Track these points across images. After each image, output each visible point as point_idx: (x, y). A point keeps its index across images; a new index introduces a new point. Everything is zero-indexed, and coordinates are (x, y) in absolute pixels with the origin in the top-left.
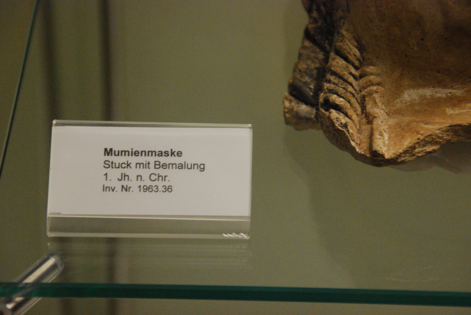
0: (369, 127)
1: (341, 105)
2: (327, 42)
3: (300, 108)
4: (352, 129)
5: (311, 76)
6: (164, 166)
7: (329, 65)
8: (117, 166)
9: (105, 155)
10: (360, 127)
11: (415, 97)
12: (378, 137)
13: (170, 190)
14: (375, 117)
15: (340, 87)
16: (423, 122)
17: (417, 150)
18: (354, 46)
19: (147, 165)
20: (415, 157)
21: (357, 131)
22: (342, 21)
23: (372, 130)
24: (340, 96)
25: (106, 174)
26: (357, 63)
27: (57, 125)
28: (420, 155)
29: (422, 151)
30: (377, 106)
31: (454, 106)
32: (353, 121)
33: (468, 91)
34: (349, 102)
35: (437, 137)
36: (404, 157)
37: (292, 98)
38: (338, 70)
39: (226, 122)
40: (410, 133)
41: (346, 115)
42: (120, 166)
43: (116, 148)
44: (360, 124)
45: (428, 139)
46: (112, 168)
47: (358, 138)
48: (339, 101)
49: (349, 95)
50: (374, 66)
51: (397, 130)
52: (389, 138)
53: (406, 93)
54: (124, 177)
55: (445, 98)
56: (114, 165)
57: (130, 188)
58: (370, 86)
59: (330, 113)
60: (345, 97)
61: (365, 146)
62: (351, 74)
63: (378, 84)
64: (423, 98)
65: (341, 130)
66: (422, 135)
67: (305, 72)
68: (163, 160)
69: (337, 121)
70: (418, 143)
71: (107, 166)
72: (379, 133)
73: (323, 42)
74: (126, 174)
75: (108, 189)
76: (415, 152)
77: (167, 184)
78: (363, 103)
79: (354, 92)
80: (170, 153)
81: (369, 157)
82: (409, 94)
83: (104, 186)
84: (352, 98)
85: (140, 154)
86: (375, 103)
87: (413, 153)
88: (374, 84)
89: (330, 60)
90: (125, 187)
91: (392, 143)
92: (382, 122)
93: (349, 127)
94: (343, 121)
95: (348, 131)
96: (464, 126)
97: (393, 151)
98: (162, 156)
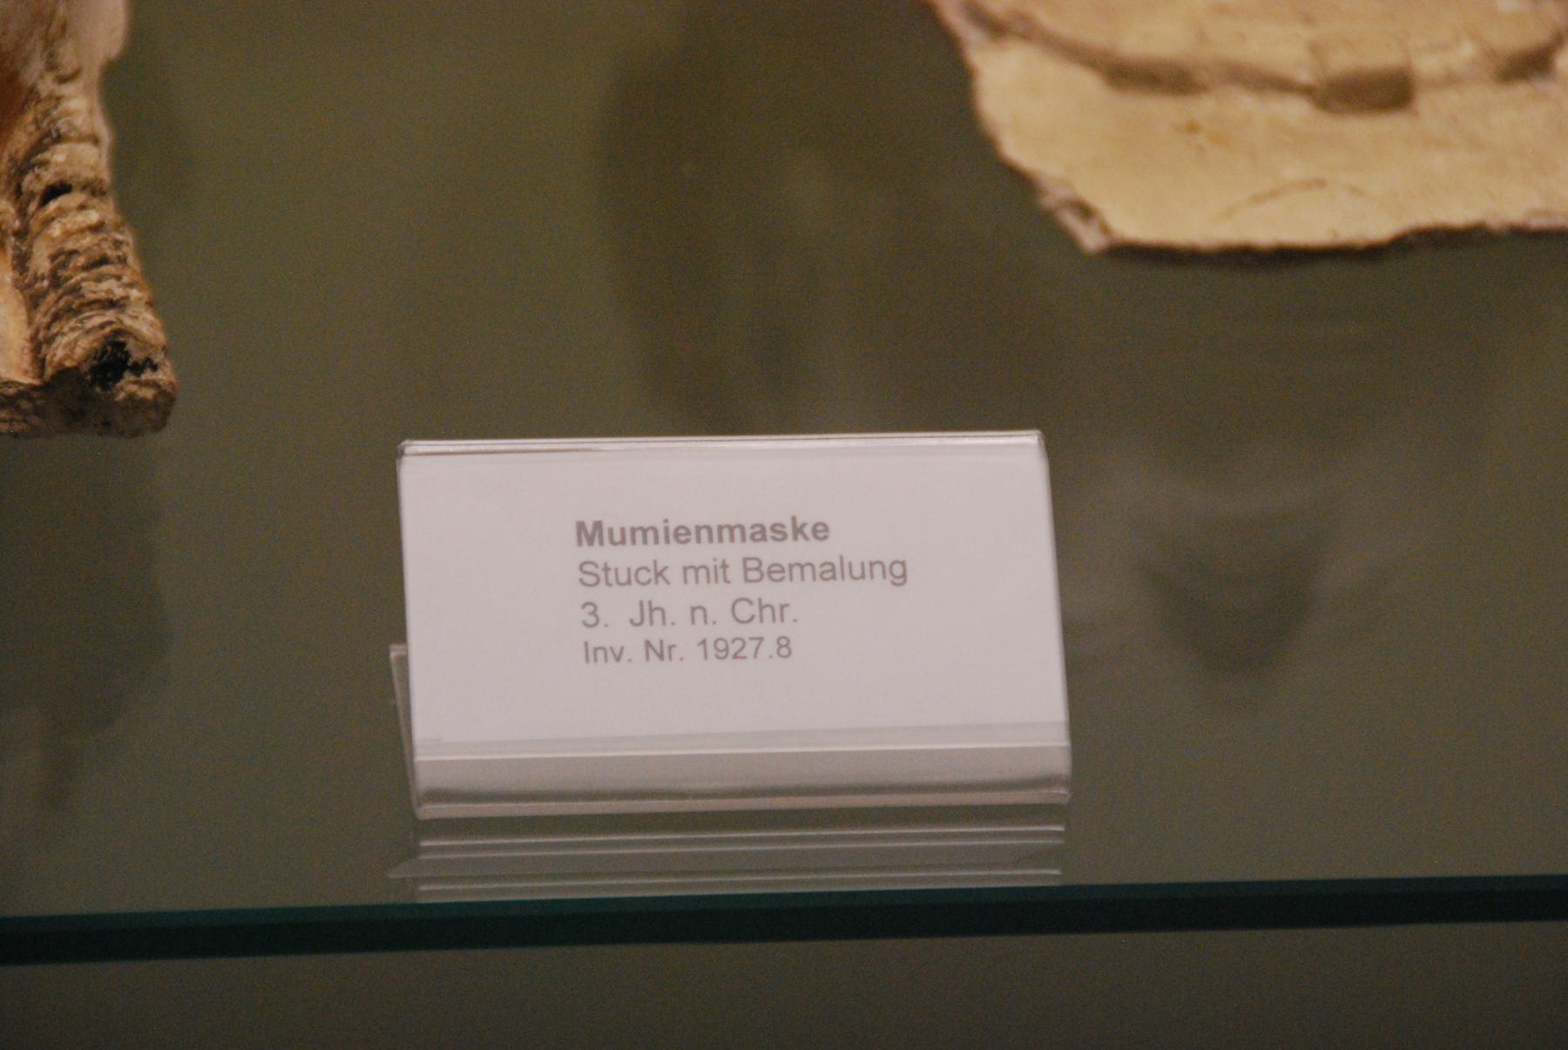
9: (580, 542)
19: (720, 572)
43: (615, 520)
46: (609, 584)
54: (649, 612)
56: (612, 575)
57: (670, 648)
71: (590, 579)
74: (654, 605)
80: (789, 530)
85: (693, 536)
90: (657, 645)
98: (764, 539)
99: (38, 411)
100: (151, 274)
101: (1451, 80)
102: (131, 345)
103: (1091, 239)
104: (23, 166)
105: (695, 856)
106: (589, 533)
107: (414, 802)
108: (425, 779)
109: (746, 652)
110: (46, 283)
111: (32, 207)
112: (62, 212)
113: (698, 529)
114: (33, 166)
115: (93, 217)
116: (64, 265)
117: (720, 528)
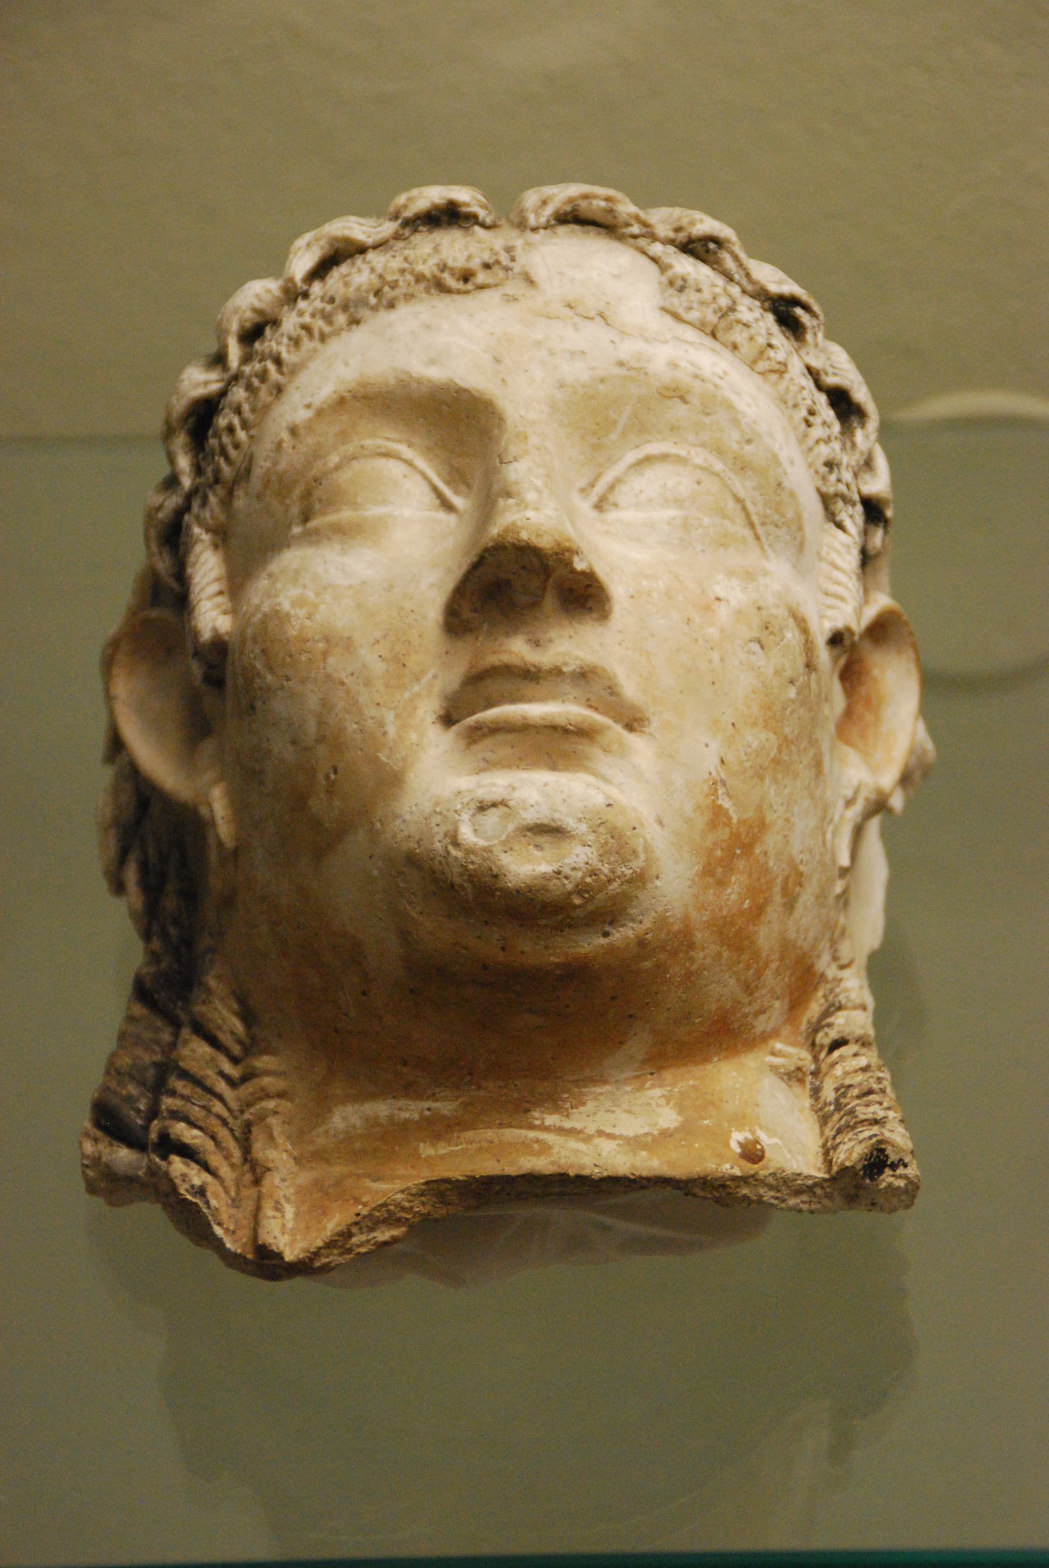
0: (250, 1192)
1: (194, 1144)
4: (216, 1199)
5: (142, 1083)
7: (175, 1053)
11: (356, 1121)
12: (270, 1213)
14: (269, 1169)
15: (195, 1104)
16: (369, 1176)
17: (355, 1240)
20: (352, 1256)
21: (230, 1202)
22: (209, 957)
23: (259, 1198)
24: (192, 1124)
26: (236, 1050)
28: (363, 1250)
29: (368, 1241)
30: (275, 1144)
31: (437, 1137)
34: (213, 1138)
35: (399, 1209)
36: (328, 1257)
37: (99, 1133)
40: (339, 1202)
41: (206, 1167)
44: (237, 1186)
45: (377, 1214)
47: (230, 1217)
48: (190, 1136)
49: (214, 1122)
51: (315, 1196)
52: (297, 1214)
53: (337, 1113)
55: (417, 1122)
58: (261, 1099)
59: (170, 1163)
61: (244, 1235)
62: (222, 1074)
63: (282, 1095)
64: (372, 1122)
66: (365, 1205)
69: (184, 1181)
70: (356, 1223)
72: (273, 1205)
73: (171, 1005)
76: (352, 1245)
78: (247, 1139)
79: (225, 1114)
81: (252, 1260)
82: (344, 1114)
84: (220, 1128)
86: (271, 1137)
87: (348, 1246)
88: (271, 1094)
89: (179, 1046)
91: (302, 1226)
92: (283, 1180)
93: (208, 1194)
94: (197, 1181)
95: (207, 1203)
97: (301, 1245)
99: (827, 1196)
104: (817, 1027)
110: (832, 1108)
112: (842, 1058)
114: (822, 1027)
115: (863, 1061)
116: (844, 1095)
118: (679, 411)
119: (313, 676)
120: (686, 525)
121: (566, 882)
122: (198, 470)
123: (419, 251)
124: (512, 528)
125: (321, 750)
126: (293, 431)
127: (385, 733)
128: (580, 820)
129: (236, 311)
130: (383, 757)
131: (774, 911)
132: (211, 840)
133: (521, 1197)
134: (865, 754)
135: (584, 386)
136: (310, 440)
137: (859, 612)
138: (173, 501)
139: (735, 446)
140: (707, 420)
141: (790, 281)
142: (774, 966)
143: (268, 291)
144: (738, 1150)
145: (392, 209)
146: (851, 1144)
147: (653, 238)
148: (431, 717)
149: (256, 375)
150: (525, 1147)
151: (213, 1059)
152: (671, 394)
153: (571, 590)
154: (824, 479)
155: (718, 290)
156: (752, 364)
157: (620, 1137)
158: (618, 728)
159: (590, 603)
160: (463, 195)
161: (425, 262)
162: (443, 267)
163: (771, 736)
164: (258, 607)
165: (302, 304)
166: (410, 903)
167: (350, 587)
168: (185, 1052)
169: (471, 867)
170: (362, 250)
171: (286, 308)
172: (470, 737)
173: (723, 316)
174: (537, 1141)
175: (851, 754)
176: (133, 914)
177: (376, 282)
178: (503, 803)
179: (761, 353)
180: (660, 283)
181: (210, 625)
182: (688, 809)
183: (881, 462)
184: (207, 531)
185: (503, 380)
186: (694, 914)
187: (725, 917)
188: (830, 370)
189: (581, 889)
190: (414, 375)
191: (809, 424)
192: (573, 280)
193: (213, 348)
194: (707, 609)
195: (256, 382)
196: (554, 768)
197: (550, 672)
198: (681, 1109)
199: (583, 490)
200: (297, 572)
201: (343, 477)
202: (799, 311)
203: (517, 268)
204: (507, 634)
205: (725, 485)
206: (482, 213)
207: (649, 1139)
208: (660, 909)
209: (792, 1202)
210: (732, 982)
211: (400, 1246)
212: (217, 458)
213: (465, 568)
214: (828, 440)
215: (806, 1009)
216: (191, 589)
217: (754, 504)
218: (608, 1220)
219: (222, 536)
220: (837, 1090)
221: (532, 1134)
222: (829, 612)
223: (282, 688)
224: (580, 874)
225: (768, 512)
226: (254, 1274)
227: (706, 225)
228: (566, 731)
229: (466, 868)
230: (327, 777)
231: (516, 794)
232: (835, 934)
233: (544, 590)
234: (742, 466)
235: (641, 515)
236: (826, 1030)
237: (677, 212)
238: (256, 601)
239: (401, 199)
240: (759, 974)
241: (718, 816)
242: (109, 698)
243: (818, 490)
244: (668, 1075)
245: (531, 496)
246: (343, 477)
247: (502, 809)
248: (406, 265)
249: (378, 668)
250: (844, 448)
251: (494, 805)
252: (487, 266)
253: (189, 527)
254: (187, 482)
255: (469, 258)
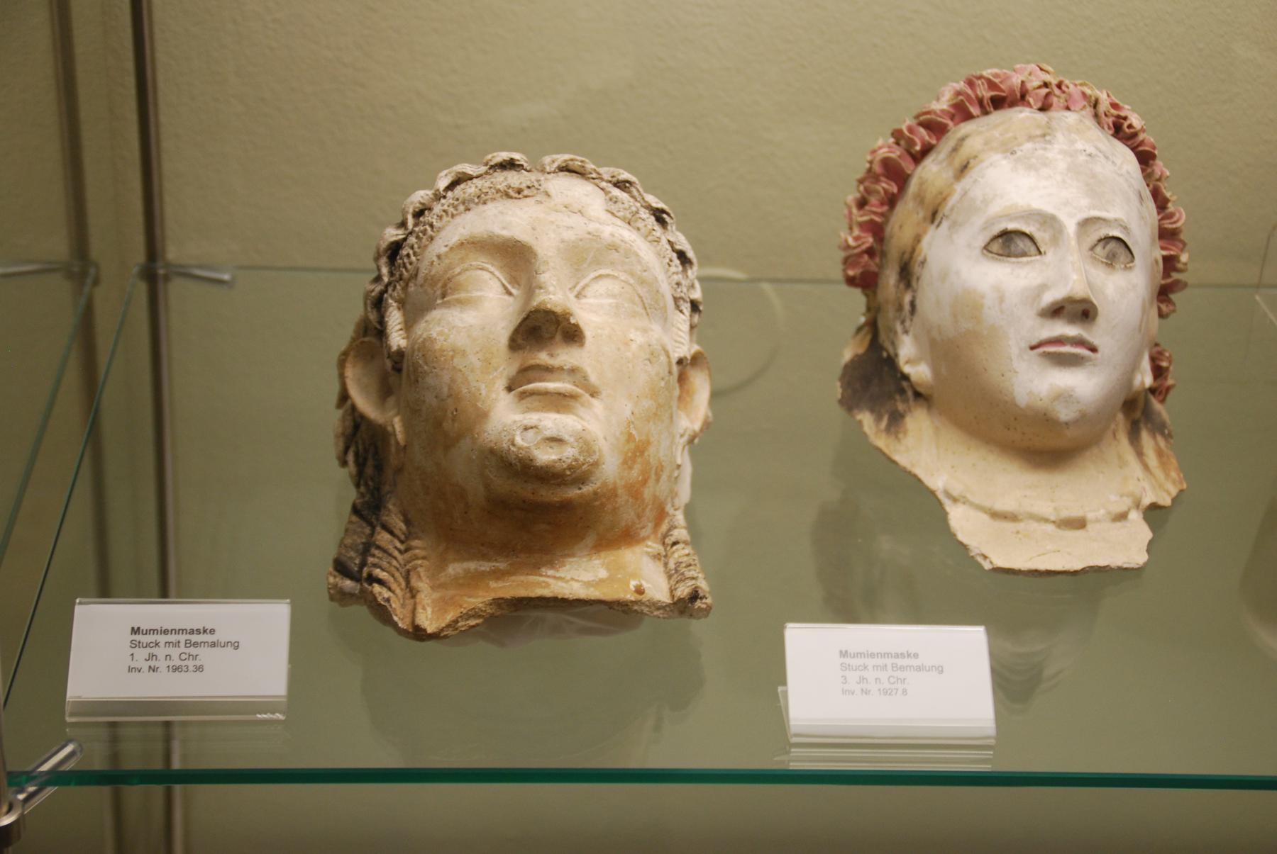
0: (412, 601)
2: (374, 517)
3: (344, 584)
5: (357, 551)
6: (196, 644)
7: (373, 539)
8: (145, 645)
10: (404, 601)
12: (421, 611)
13: (201, 670)
17: (460, 624)
18: (400, 519)
22: (388, 496)
24: (383, 570)
25: (132, 655)
26: (403, 537)
27: (80, 603)
28: (463, 629)
29: (465, 625)
31: (498, 579)
32: (397, 596)
33: (510, 564)
34: (393, 576)
37: (336, 574)
38: (382, 544)
39: (264, 598)
41: (390, 589)
42: (148, 645)
43: (144, 627)
45: (470, 613)
46: (850, 670)
48: (383, 575)
49: (393, 569)
50: (419, 539)
52: (433, 612)
54: (152, 656)
56: (141, 644)
57: (158, 668)
58: (414, 560)
59: (373, 587)
60: (388, 570)
61: (408, 620)
62: (396, 548)
63: (424, 558)
64: (467, 571)
65: (384, 606)
66: (465, 608)
67: (351, 547)
68: (195, 638)
70: (461, 617)
71: (844, 669)
75: (134, 670)
77: (198, 663)
79: (398, 566)
80: (202, 631)
83: (129, 667)
89: (376, 534)
90: (864, 690)
93: (391, 602)
95: (391, 605)
96: (507, 599)
98: (193, 634)
99: (671, 611)
100: (703, 570)
101: (1097, 521)
102: (700, 591)
103: (987, 566)
104: (665, 536)
105: (875, 757)
106: (844, 654)
107: (789, 737)
108: (793, 730)
109: (893, 693)
110: (673, 572)
111: (668, 548)
112: (677, 550)
113: (878, 654)
114: (668, 536)
115: (687, 551)
116: (679, 566)
117: (884, 654)
118: (615, 256)
119: (447, 367)
120: (617, 307)
121: (563, 464)
122: (391, 274)
123: (498, 180)
124: (543, 303)
125: (450, 401)
126: (439, 257)
127: (480, 394)
128: (571, 436)
129: (412, 203)
130: (479, 404)
131: (651, 482)
132: (393, 442)
133: (536, 607)
134: (688, 416)
135: (573, 242)
136: (447, 261)
137: (689, 350)
138: (379, 288)
139: (639, 273)
140: (627, 260)
141: (661, 203)
142: (650, 507)
143: (427, 195)
144: (634, 589)
145: (485, 161)
146: (683, 588)
147: (602, 179)
148: (502, 387)
149: (421, 232)
150: (539, 584)
151: (392, 541)
152: (611, 248)
153: (567, 332)
154: (675, 290)
155: (631, 204)
156: (646, 237)
157: (582, 581)
158: (587, 396)
159: (576, 339)
160: (516, 156)
161: (500, 184)
162: (509, 187)
163: (654, 403)
164: (421, 336)
165: (443, 201)
166: (490, 471)
167: (465, 327)
168: (379, 537)
169: (520, 455)
170: (471, 178)
171: (435, 203)
172: (520, 397)
173: (633, 216)
174: (544, 582)
175: (682, 415)
176: (351, 476)
177: (478, 192)
178: (536, 427)
179: (650, 233)
180: (606, 199)
181: (397, 344)
182: (618, 434)
183: (697, 285)
184: (396, 302)
185: (536, 238)
186: (618, 481)
187: (631, 484)
188: (678, 243)
189: (570, 468)
190: (496, 234)
191: (670, 265)
192: (567, 196)
193: (399, 220)
194: (626, 344)
195: (421, 235)
196: (558, 412)
197: (558, 368)
198: (608, 569)
199: (570, 289)
200: (440, 320)
201: (462, 278)
202: (665, 216)
203: (542, 189)
204: (539, 351)
205: (635, 290)
206: (525, 165)
207: (594, 583)
208: (604, 479)
209: (656, 613)
210: (632, 513)
211: (477, 628)
212: (401, 269)
213: (519, 321)
214: (677, 273)
215: (536, 568)
216: (388, 327)
217: (647, 299)
218: (572, 619)
219: (402, 304)
220: (676, 564)
221: (541, 579)
222: (677, 350)
223: (432, 372)
224: (570, 461)
225: (652, 303)
226: (410, 638)
227: (625, 175)
228: (565, 396)
229: (517, 456)
230: (452, 413)
231: (542, 423)
232: (674, 494)
233: (557, 331)
234: (642, 282)
235: (596, 301)
236: (670, 537)
237: (612, 169)
238: (420, 333)
239: (489, 157)
240: (644, 510)
241: (630, 437)
242: (342, 377)
243: (673, 295)
244: (603, 554)
245: (551, 289)
246: (462, 278)
247: (535, 430)
248: (492, 186)
249: (478, 364)
250: (683, 278)
251: (532, 428)
252: (529, 187)
253: (387, 300)
254: (386, 279)
255: (521, 183)
